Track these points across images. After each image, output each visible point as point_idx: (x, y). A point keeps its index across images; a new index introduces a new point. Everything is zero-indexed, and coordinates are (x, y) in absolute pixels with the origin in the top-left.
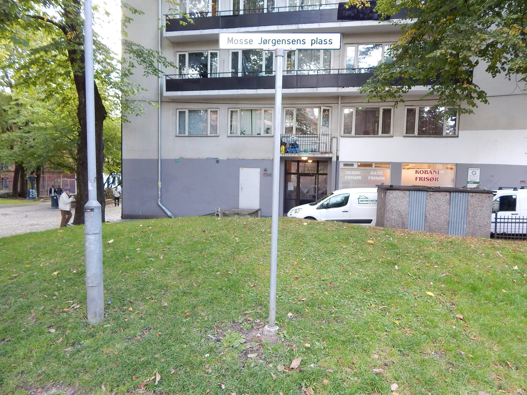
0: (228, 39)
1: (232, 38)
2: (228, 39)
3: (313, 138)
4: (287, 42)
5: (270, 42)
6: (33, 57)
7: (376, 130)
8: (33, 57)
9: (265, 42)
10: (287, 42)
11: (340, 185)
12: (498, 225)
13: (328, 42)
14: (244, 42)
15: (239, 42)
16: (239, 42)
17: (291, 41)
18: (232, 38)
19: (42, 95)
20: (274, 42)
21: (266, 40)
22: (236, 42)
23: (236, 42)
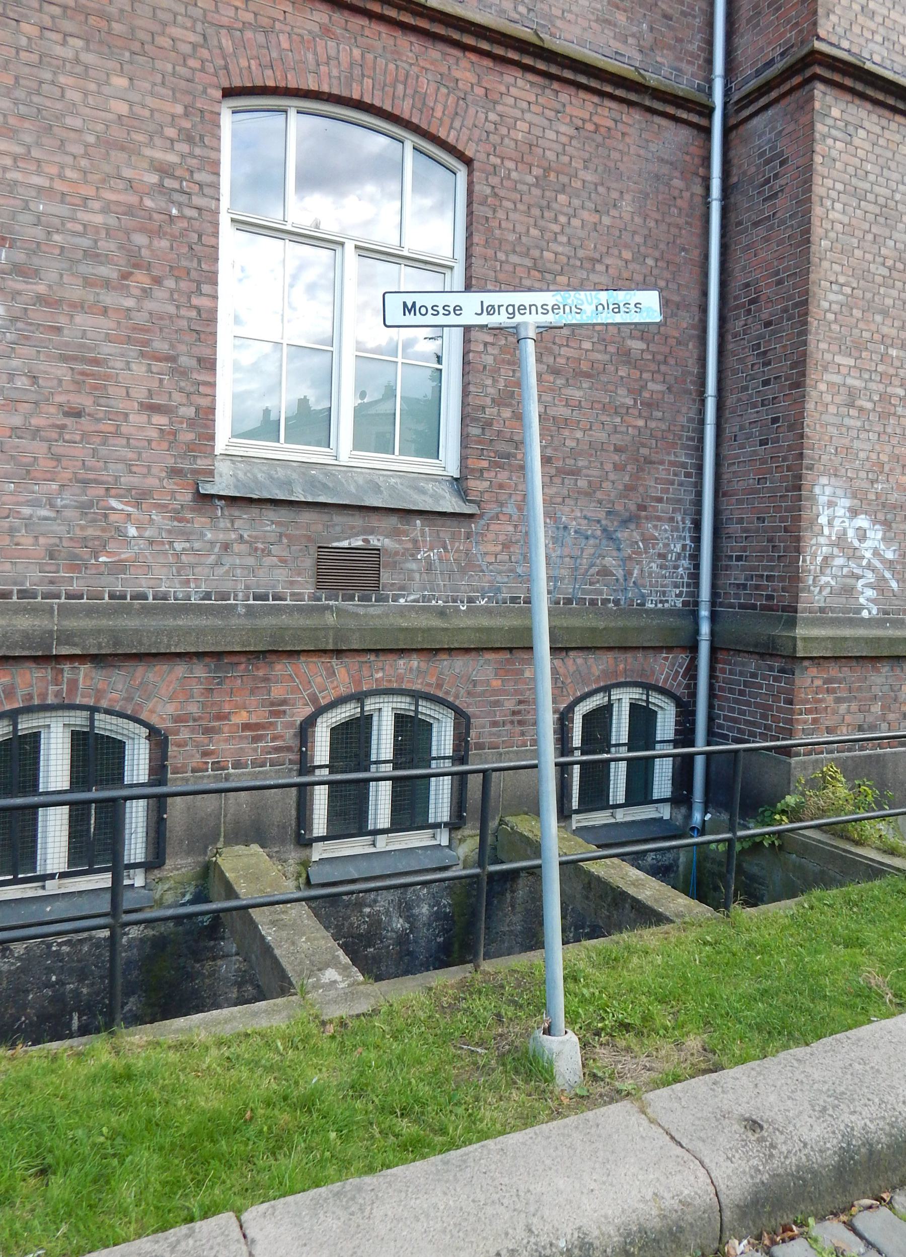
0: (405, 304)
1: (414, 303)
2: (405, 304)
3: (49, 856)
4: (540, 310)
5: (503, 309)
6: (839, 877)
7: (870, 92)
8: (839, 877)
9: (491, 310)
10: (540, 310)
11: (701, 98)
12: (176, 806)
13: (442, 311)
14: (442, 311)
15: (430, 311)
16: (430, 311)
17: (549, 308)
18: (414, 303)
19: (825, 1101)
20: (510, 310)
21: (493, 307)
22: (423, 311)
23: (423, 311)
